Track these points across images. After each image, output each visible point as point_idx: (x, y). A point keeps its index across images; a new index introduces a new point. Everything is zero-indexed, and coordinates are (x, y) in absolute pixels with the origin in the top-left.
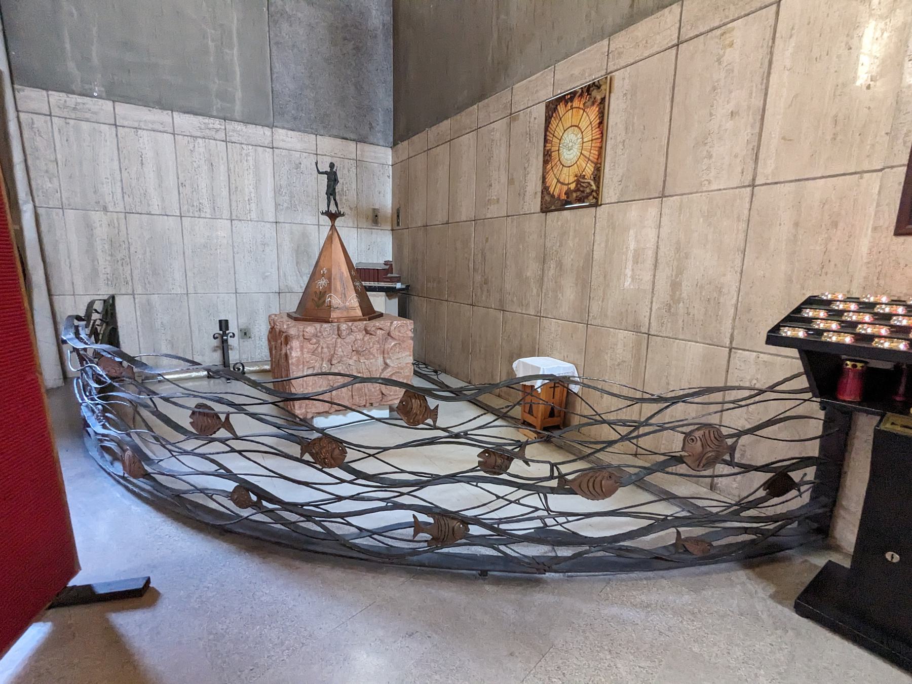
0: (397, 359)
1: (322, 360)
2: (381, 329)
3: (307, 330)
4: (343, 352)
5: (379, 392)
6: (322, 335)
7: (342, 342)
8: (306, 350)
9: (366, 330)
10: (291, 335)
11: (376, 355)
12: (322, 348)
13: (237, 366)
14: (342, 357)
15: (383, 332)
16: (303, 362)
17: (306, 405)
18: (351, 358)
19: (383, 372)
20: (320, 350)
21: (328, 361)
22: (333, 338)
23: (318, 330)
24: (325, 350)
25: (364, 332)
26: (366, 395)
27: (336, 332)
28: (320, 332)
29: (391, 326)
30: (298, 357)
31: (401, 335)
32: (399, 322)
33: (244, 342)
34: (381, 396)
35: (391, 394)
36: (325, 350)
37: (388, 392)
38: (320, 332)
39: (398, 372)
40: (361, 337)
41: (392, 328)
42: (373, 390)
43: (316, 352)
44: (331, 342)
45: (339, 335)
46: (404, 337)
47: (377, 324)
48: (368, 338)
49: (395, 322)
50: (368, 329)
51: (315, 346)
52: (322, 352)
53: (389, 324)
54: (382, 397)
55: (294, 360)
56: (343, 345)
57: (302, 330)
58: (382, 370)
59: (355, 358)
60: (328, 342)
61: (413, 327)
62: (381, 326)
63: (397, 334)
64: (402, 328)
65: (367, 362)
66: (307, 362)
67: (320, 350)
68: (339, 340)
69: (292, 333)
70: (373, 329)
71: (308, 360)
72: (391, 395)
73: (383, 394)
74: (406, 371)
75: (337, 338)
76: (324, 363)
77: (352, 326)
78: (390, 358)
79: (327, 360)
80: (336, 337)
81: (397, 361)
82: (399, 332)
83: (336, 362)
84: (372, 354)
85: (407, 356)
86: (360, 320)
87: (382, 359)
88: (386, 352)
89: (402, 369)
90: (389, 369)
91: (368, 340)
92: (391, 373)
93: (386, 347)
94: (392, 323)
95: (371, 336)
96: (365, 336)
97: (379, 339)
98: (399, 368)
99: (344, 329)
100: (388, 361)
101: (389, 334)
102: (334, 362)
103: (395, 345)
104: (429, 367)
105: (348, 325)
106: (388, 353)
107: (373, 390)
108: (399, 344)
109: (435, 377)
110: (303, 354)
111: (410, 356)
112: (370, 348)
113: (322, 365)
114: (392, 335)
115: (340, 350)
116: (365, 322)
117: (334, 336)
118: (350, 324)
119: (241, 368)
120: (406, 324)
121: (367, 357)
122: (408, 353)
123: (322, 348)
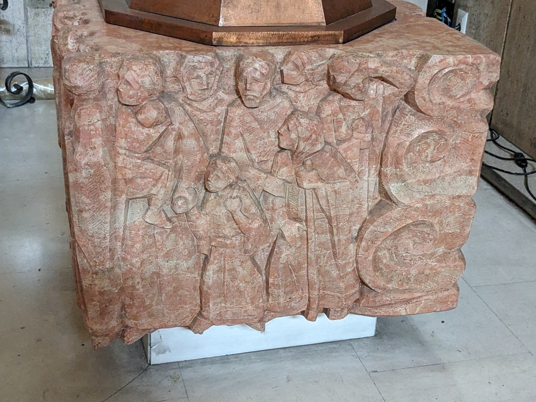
0: (425, 182)
1: (178, 172)
2: (382, 79)
3: (129, 76)
4: (248, 150)
5: (351, 279)
6: (184, 88)
7: (248, 119)
8: (122, 142)
9: (330, 79)
10: (76, 87)
11: (356, 167)
12: (180, 137)
13: (16, 80)
14: (242, 166)
15: (390, 90)
16: (115, 181)
17: (123, 308)
18: (271, 173)
19: (372, 222)
20: (170, 143)
21: (198, 179)
22: (220, 101)
23: (169, 72)
24: (190, 143)
25: (324, 85)
26: (310, 285)
27: (231, 82)
28: (177, 79)
29: (419, 67)
30: (97, 166)
31: (450, 103)
32: (451, 59)
33: (37, 15)
34: (357, 287)
35: (390, 286)
36: (190, 143)
37: (381, 282)
38: (177, 79)
39: (423, 223)
40: (314, 103)
41: (423, 79)
42: (335, 273)
43: (159, 150)
44: (209, 116)
45: (237, 92)
46: (458, 109)
47: (373, 64)
48: (336, 105)
49: (435, 58)
50: (341, 79)
51: (155, 133)
52: (177, 151)
53: (414, 61)
54: (361, 293)
55: (84, 173)
56: (251, 131)
57: (114, 71)
58: (370, 213)
59: (285, 172)
60: (202, 116)
61: (495, 76)
62: (383, 71)
63: (437, 98)
64: (455, 80)
65: (323, 188)
66: (128, 181)
67: (170, 143)
68: (238, 112)
69: (79, 82)
70: (357, 80)
71: (129, 175)
72: (390, 291)
73: (363, 283)
74: (451, 219)
75: (231, 104)
76: (184, 185)
77: (285, 61)
78: (401, 178)
79: (193, 175)
80: (228, 98)
81: (426, 188)
82: (446, 91)
83: (221, 184)
84: (343, 162)
85: (460, 173)
86: (315, 41)
87: (374, 179)
88: (390, 158)
89: (436, 213)
90: (395, 213)
91: (334, 114)
92: (398, 225)
93: (393, 141)
94: (424, 59)
95: (346, 102)
96: (324, 99)
97: (372, 115)
98: (425, 211)
99: (257, 75)
100: (393, 188)
101: (408, 98)
102: (215, 184)
103: (423, 137)
104: (501, 141)
105: (271, 61)
106: (397, 163)
107: (335, 273)
108: (441, 134)
109: (517, 183)
110: (113, 153)
111: (470, 173)
112: (340, 142)
113: (175, 190)
114: (419, 101)
115: (239, 143)
116: (330, 51)
117: (221, 94)
118: (279, 53)
119: (25, 86)
120: (475, 66)
121: (325, 172)
122: (464, 165)
123: (180, 137)
